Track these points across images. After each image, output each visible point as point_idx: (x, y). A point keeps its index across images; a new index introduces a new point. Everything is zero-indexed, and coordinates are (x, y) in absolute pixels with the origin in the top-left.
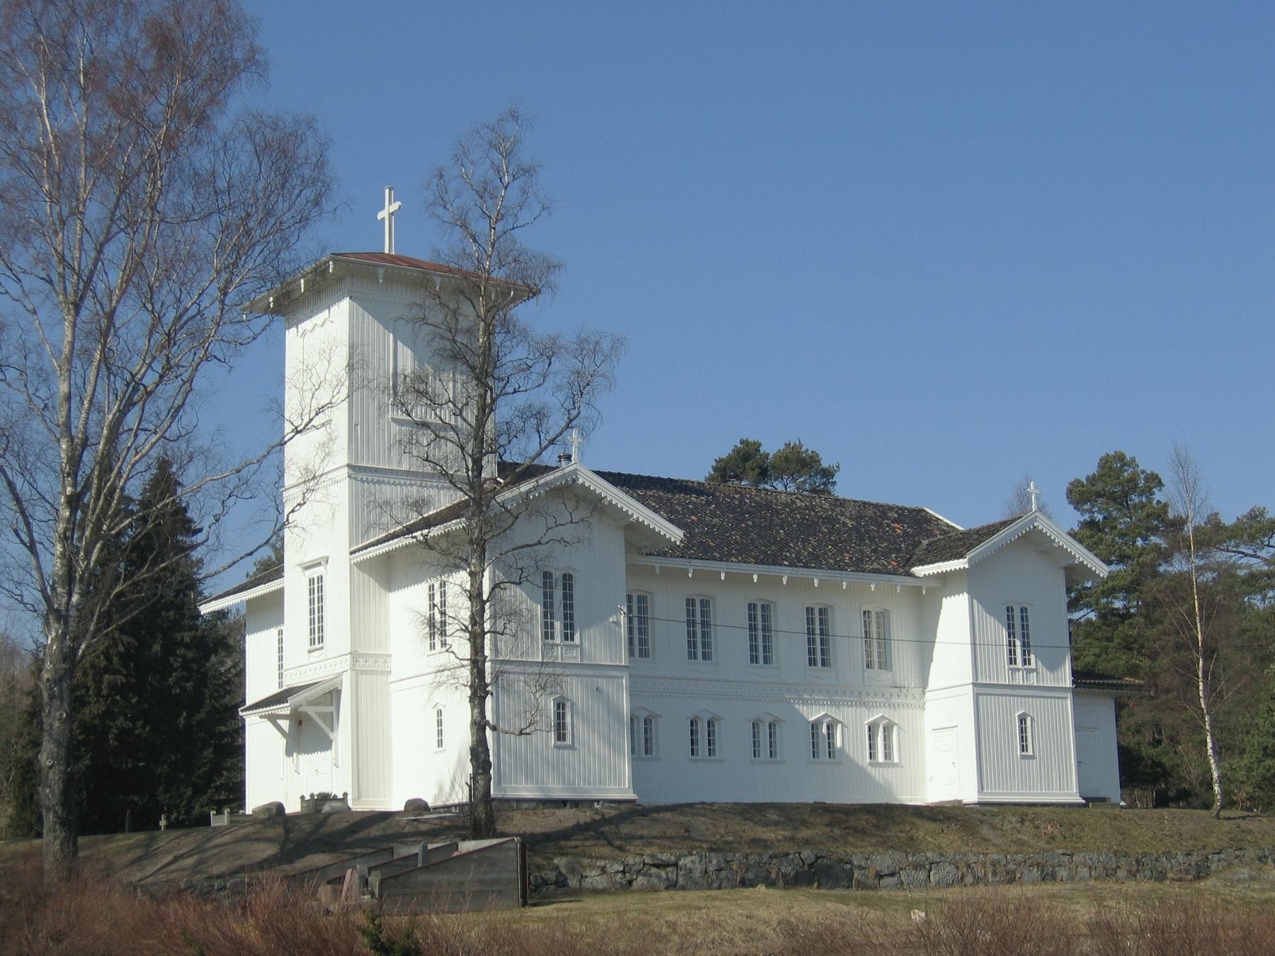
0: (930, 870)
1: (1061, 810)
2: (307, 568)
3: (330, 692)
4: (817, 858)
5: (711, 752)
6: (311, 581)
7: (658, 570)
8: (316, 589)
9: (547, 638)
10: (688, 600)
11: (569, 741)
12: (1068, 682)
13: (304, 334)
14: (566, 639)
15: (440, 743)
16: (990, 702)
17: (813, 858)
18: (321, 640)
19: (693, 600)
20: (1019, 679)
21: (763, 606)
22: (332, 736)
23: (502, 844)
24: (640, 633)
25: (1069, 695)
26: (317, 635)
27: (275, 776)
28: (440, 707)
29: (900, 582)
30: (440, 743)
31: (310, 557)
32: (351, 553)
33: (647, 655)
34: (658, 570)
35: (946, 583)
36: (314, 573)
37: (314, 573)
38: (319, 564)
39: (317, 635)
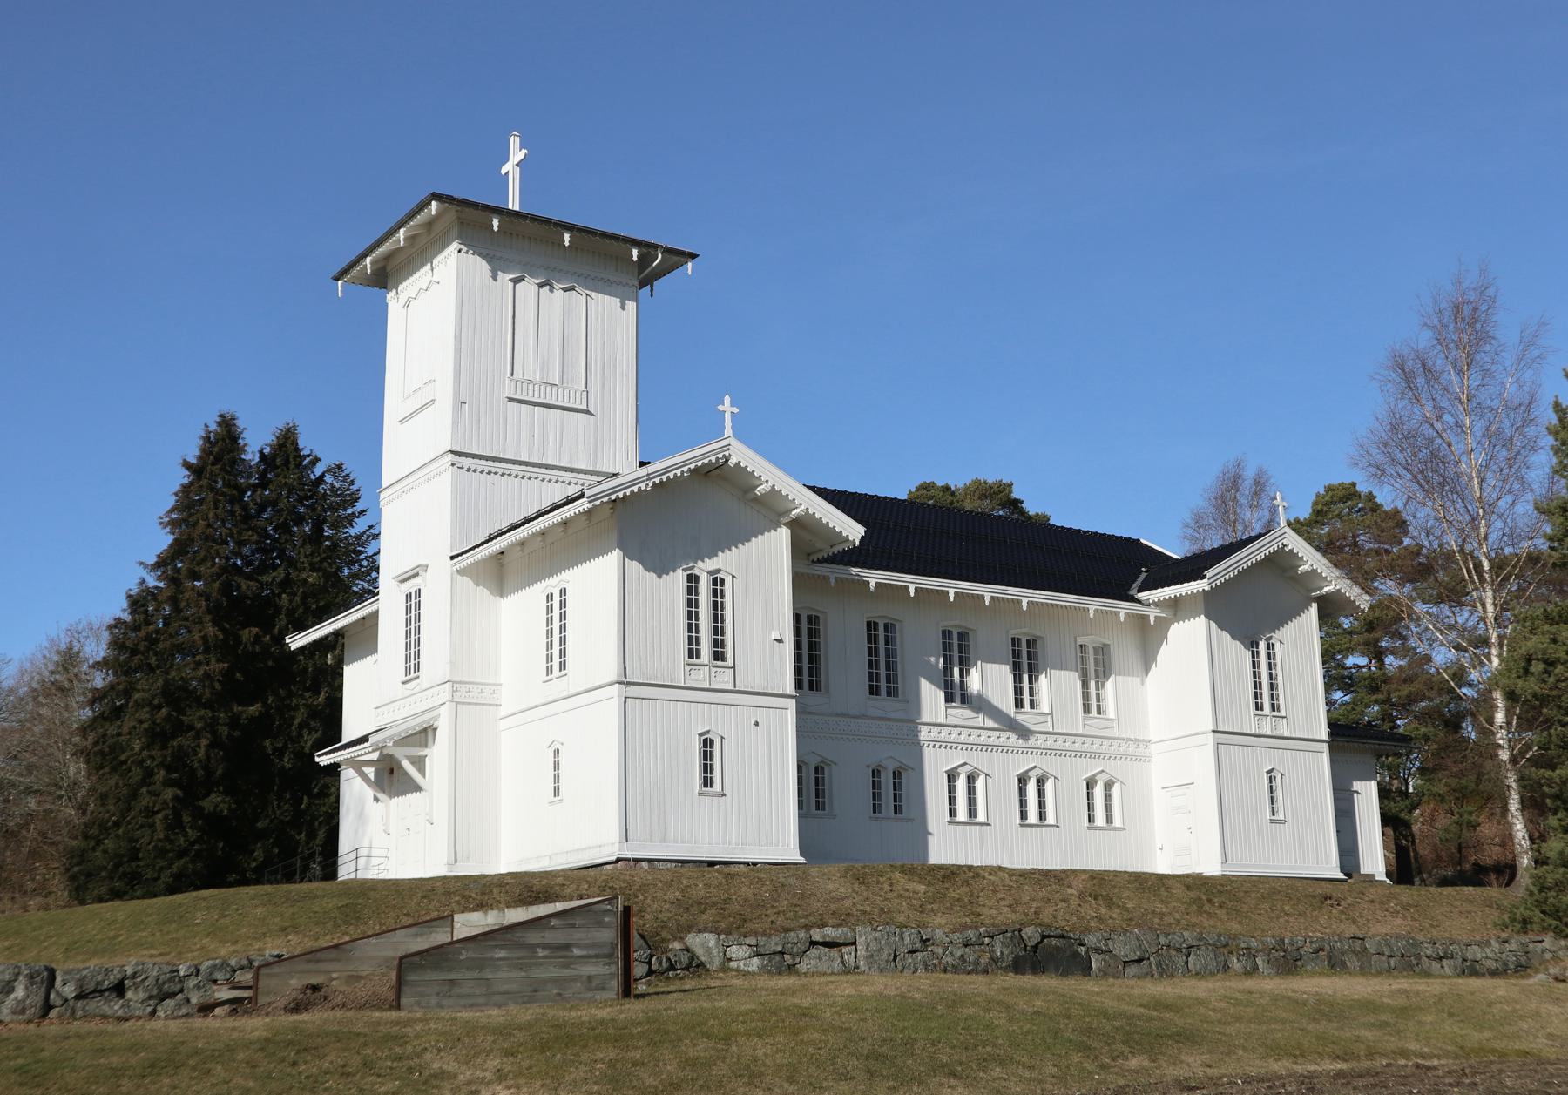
0: (1188, 956)
1: (1328, 885)
2: (403, 581)
3: (425, 730)
4: (1044, 937)
5: (898, 810)
6: (408, 597)
7: (832, 581)
8: (414, 603)
9: (691, 656)
10: (869, 624)
11: (717, 787)
12: (1324, 733)
13: (407, 305)
14: (716, 659)
15: (556, 791)
16: (1231, 753)
17: (1037, 938)
18: (417, 667)
19: (876, 624)
20: (1266, 727)
21: (960, 634)
22: (96, 649)
23: (630, 922)
24: (810, 661)
25: (1326, 746)
26: (413, 664)
27: (383, 839)
28: (558, 746)
29: (1123, 609)
30: (556, 791)
31: (405, 567)
32: (452, 558)
33: (819, 689)
34: (832, 581)
35: (1177, 608)
36: (410, 587)
37: (410, 587)
38: (417, 575)
39: (413, 664)
